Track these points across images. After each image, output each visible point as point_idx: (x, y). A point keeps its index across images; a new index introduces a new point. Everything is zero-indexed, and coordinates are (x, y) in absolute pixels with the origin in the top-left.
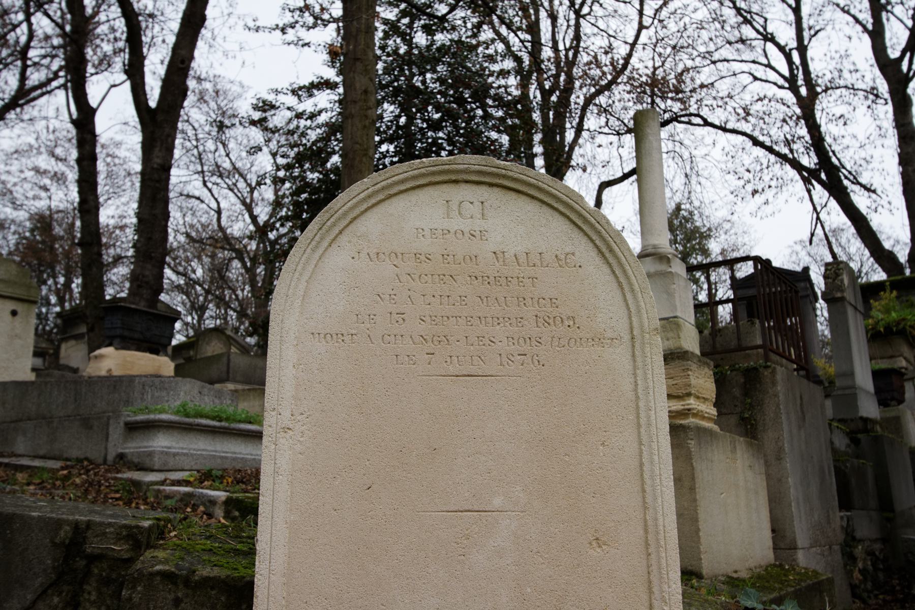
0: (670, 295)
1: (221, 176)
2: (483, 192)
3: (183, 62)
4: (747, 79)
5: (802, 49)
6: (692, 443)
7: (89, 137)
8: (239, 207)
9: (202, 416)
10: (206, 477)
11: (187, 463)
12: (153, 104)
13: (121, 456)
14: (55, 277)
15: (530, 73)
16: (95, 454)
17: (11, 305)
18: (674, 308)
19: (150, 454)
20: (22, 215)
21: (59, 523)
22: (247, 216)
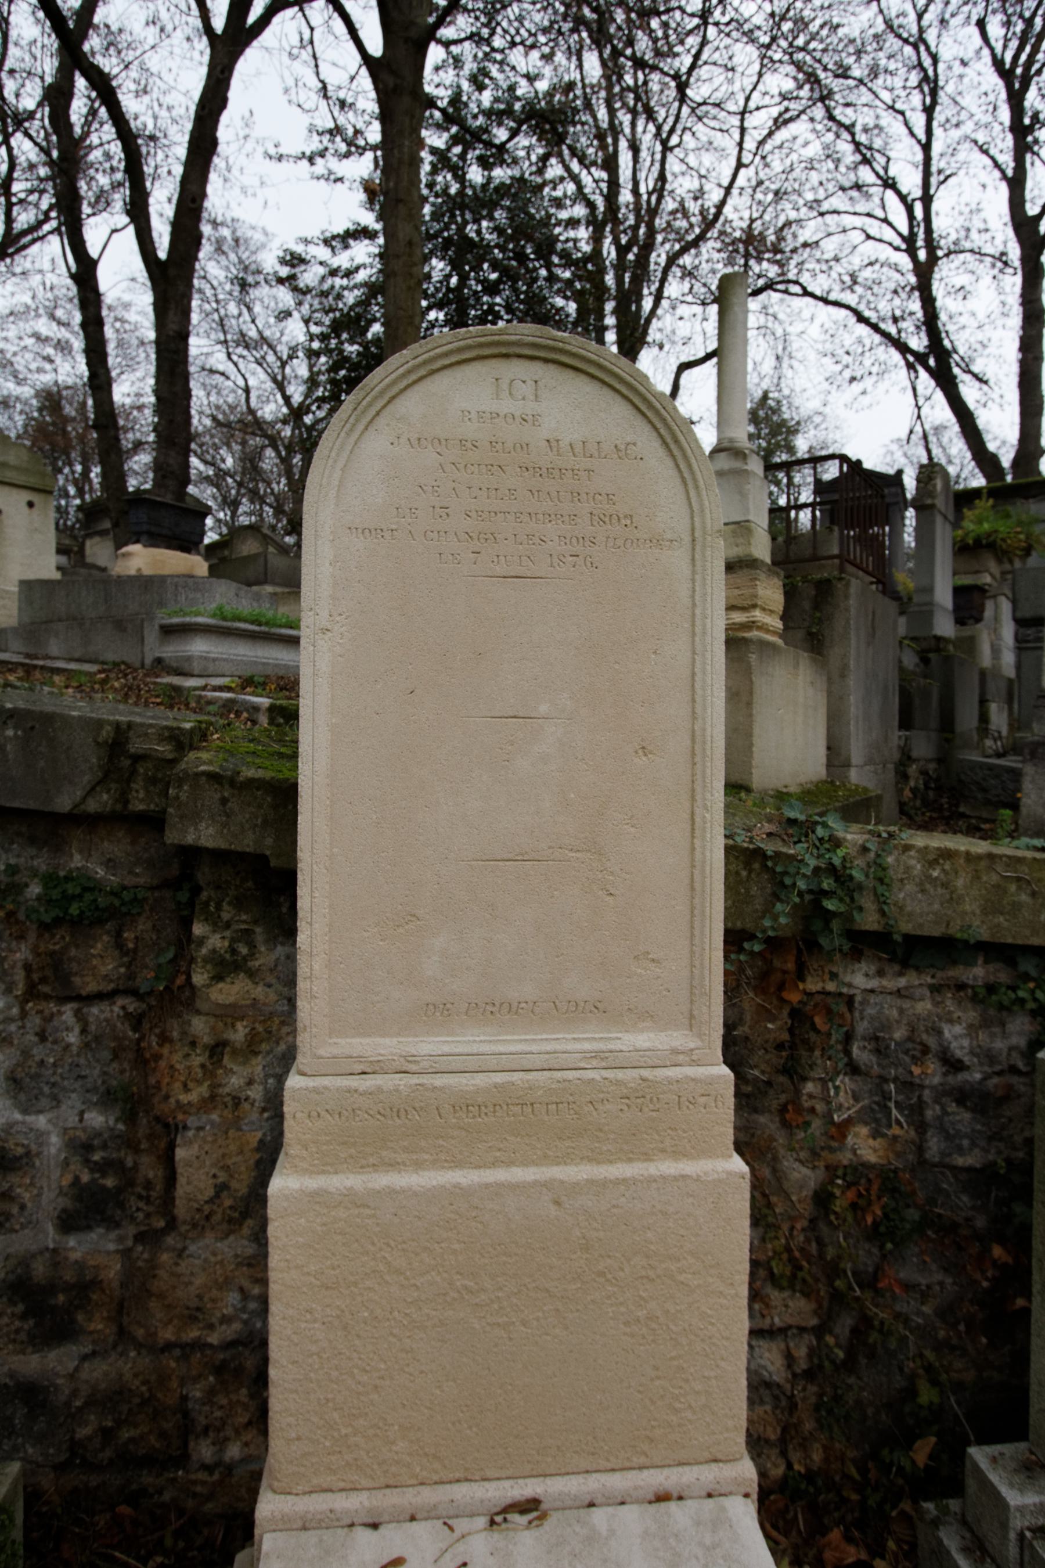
2: (537, 369)
3: (194, 201)
4: (857, 237)
5: (927, 199)
6: (753, 658)
8: (269, 385)
9: (240, 619)
10: (248, 683)
12: (162, 255)
13: (159, 661)
16: (133, 659)
17: (26, 496)
18: (747, 510)
19: (189, 659)
20: (26, 392)
21: (100, 724)
22: (279, 396)
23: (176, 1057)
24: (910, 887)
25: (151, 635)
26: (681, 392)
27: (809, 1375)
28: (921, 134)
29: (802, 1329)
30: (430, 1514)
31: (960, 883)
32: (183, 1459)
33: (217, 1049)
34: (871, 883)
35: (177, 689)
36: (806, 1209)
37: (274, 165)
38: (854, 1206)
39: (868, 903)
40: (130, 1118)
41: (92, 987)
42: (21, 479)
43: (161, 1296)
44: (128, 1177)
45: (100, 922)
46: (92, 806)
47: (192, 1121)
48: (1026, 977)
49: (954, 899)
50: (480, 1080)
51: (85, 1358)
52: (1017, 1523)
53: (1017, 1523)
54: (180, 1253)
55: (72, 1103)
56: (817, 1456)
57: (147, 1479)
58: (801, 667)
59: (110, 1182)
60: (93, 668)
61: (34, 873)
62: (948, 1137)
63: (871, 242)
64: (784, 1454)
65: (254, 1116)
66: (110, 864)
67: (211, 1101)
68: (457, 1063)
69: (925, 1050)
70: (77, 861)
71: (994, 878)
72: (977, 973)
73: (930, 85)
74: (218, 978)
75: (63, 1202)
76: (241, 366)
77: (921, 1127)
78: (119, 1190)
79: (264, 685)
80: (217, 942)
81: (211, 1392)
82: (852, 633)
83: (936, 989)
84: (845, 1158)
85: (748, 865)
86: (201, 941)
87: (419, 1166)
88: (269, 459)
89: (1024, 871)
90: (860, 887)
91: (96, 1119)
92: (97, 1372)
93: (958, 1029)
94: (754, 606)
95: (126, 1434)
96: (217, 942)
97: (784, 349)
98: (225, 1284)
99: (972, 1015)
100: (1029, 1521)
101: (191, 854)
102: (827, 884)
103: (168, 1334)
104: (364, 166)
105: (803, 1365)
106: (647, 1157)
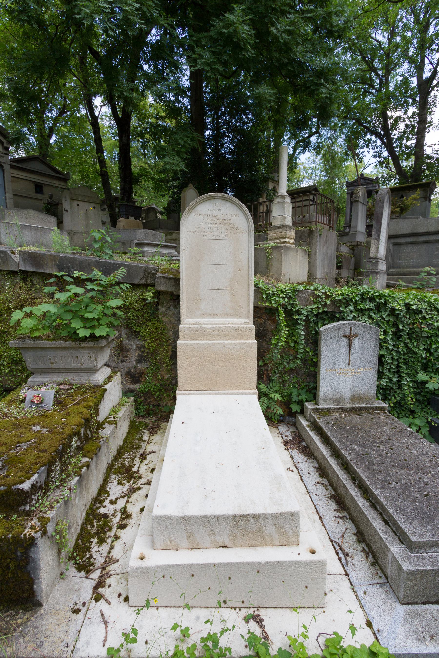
17: (93, 205)
58: (299, 253)
68: (207, 324)
87: (201, 340)
94: (286, 237)
106: (239, 340)
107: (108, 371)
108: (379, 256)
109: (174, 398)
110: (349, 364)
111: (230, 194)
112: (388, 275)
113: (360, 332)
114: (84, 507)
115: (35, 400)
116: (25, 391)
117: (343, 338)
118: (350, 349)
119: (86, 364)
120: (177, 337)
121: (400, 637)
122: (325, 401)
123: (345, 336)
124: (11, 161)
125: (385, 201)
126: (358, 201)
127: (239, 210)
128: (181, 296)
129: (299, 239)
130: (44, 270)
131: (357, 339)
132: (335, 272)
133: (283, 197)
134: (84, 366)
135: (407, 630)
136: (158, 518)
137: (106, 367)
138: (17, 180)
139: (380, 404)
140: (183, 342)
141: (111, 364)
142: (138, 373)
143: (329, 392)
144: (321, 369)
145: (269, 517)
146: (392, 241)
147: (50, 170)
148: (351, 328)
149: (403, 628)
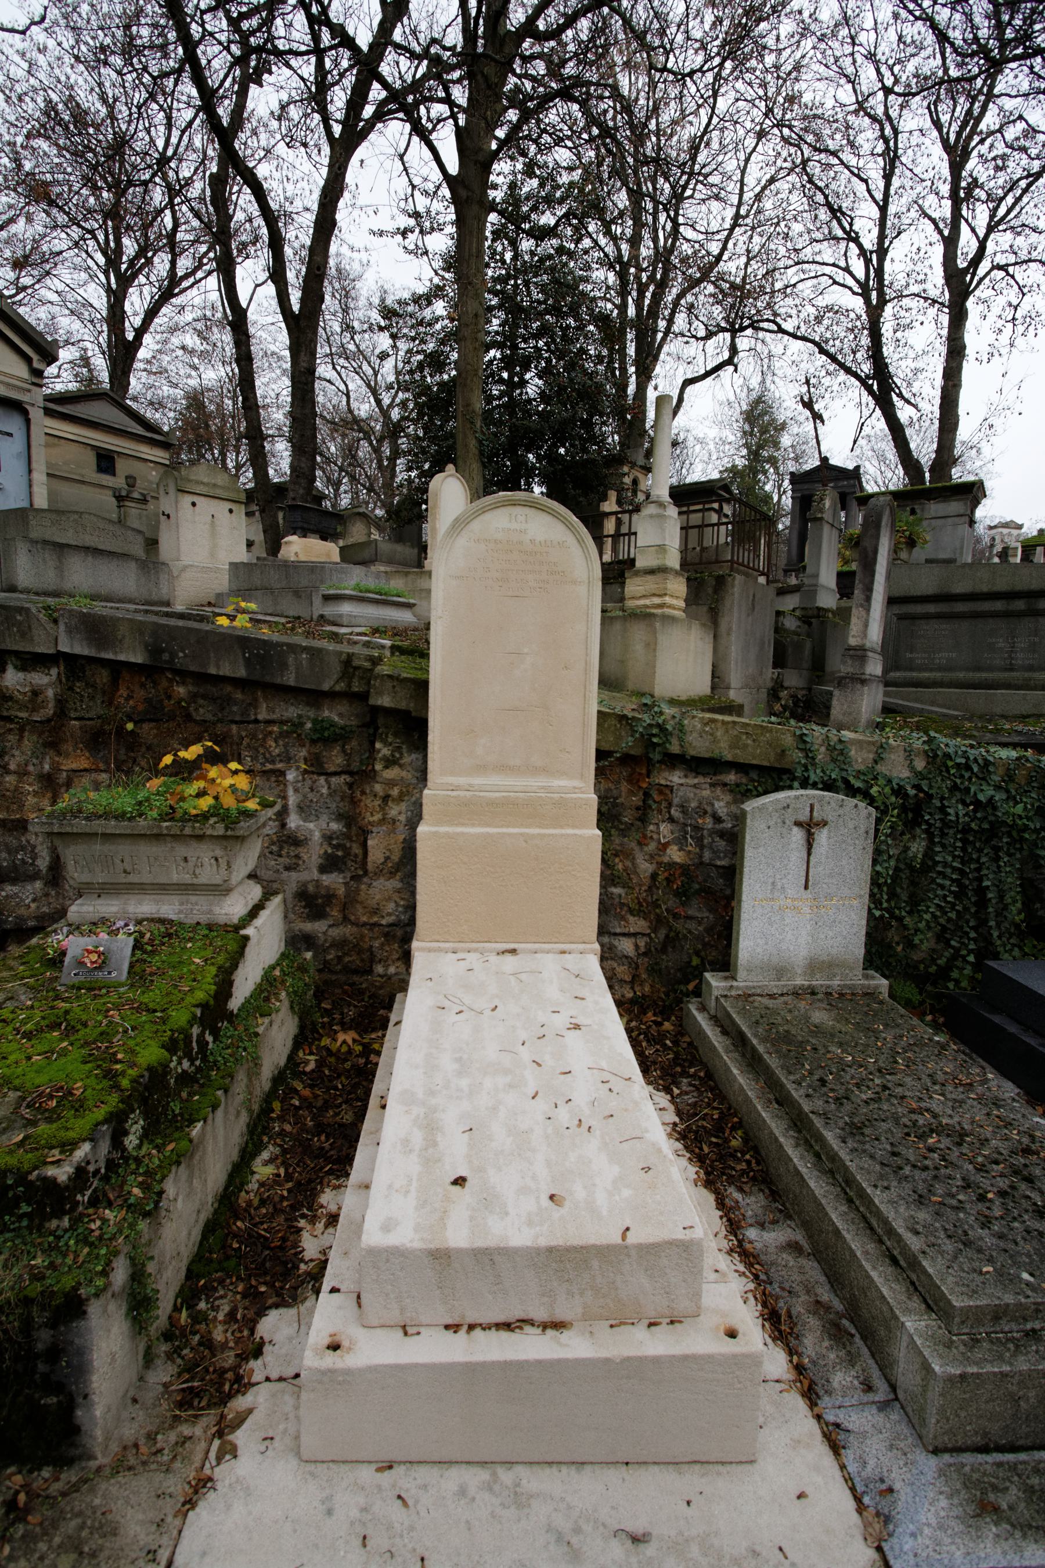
0: (663, 530)
1: (347, 359)
2: (527, 510)
3: (319, 269)
4: (825, 281)
5: (882, 252)
6: (658, 625)
7: (244, 338)
8: (364, 389)
9: (370, 592)
10: (375, 631)
11: (362, 622)
12: (296, 308)
13: (322, 616)
14: (211, 449)
15: (628, 264)
16: (305, 614)
17: (228, 505)
18: (664, 539)
19: (341, 616)
20: (179, 393)
21: (341, 653)
22: (372, 400)
23: (368, 801)
24: (695, 735)
25: (317, 601)
26: (682, 411)
27: (645, 954)
28: (879, 196)
29: (644, 935)
30: (476, 950)
31: (719, 734)
32: (370, 971)
33: (386, 798)
34: (676, 732)
35: (336, 634)
36: (647, 882)
37: (377, 240)
38: (667, 879)
39: (675, 741)
40: (348, 826)
41: (332, 769)
42: (225, 495)
43: (361, 903)
44: (347, 852)
45: (336, 741)
46: (337, 688)
47: (374, 829)
48: (753, 781)
49: (715, 741)
50: (497, 795)
51: (330, 926)
52: (716, 993)
53: (716, 993)
54: (370, 885)
55: (324, 818)
56: (647, 989)
57: (356, 978)
59: (340, 853)
60: (283, 620)
61: (309, 718)
62: (714, 852)
63: (835, 287)
64: (632, 988)
65: (401, 828)
66: (340, 715)
67: (383, 821)
68: (488, 788)
69: (705, 812)
70: (326, 713)
71: (736, 733)
72: (731, 777)
73: (891, 159)
74: (386, 767)
75: (320, 861)
76: (344, 375)
77: (702, 847)
78: (344, 857)
79: (385, 632)
80: (385, 751)
81: (382, 945)
82: (736, 609)
83: (712, 785)
84: (666, 859)
85: (620, 722)
86: (379, 751)
87: (473, 825)
88: (364, 450)
89: (750, 730)
90: (671, 734)
91: (335, 826)
92: (335, 933)
93: (722, 804)
95: (347, 959)
96: (385, 751)
97: (769, 367)
98: (389, 899)
99: (728, 798)
100: (721, 992)
101: (376, 710)
102: (655, 731)
103: (364, 919)
104: (441, 242)
105: (642, 950)
106: (562, 827)
107: (256, 892)
108: (868, 645)
109: (406, 958)
110: (806, 887)
111: (537, 490)
112: (887, 684)
113: (830, 817)
114: (194, 1215)
115: (86, 960)
116: (60, 937)
117: (795, 829)
118: (809, 854)
119: (208, 874)
120: (416, 817)
121: (927, 1531)
122: (749, 971)
123: (798, 824)
124: (49, 398)
125: (883, 523)
126: (821, 519)
127: (568, 532)
128: (431, 724)
129: (693, 599)
130: (116, 653)
131: (825, 832)
132: (770, 675)
133: (661, 505)
134: (203, 880)
135: (943, 1514)
136: (374, 1253)
137: (251, 882)
138: (56, 440)
139: (873, 978)
140: (433, 829)
141: (262, 873)
142: (322, 897)
143: (759, 950)
144: (744, 897)
145: (633, 1253)
146: (897, 609)
147: (133, 424)
148: (812, 807)
149: (933, 1509)
